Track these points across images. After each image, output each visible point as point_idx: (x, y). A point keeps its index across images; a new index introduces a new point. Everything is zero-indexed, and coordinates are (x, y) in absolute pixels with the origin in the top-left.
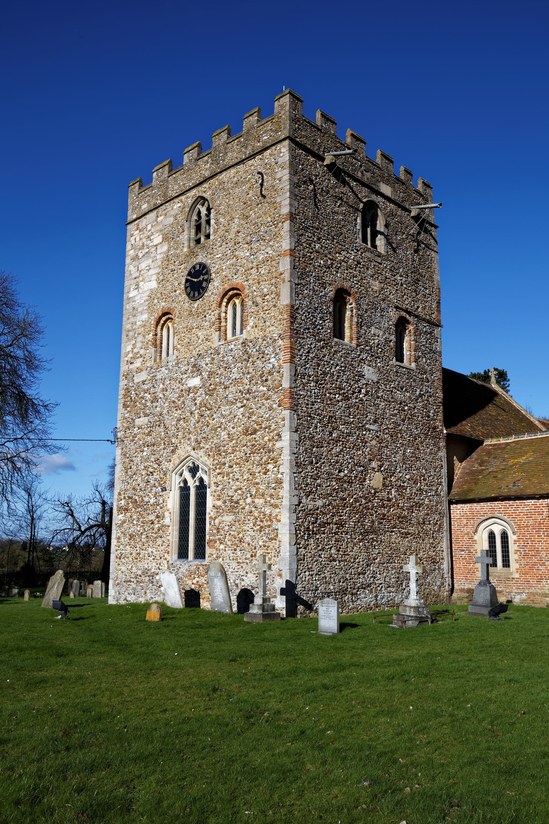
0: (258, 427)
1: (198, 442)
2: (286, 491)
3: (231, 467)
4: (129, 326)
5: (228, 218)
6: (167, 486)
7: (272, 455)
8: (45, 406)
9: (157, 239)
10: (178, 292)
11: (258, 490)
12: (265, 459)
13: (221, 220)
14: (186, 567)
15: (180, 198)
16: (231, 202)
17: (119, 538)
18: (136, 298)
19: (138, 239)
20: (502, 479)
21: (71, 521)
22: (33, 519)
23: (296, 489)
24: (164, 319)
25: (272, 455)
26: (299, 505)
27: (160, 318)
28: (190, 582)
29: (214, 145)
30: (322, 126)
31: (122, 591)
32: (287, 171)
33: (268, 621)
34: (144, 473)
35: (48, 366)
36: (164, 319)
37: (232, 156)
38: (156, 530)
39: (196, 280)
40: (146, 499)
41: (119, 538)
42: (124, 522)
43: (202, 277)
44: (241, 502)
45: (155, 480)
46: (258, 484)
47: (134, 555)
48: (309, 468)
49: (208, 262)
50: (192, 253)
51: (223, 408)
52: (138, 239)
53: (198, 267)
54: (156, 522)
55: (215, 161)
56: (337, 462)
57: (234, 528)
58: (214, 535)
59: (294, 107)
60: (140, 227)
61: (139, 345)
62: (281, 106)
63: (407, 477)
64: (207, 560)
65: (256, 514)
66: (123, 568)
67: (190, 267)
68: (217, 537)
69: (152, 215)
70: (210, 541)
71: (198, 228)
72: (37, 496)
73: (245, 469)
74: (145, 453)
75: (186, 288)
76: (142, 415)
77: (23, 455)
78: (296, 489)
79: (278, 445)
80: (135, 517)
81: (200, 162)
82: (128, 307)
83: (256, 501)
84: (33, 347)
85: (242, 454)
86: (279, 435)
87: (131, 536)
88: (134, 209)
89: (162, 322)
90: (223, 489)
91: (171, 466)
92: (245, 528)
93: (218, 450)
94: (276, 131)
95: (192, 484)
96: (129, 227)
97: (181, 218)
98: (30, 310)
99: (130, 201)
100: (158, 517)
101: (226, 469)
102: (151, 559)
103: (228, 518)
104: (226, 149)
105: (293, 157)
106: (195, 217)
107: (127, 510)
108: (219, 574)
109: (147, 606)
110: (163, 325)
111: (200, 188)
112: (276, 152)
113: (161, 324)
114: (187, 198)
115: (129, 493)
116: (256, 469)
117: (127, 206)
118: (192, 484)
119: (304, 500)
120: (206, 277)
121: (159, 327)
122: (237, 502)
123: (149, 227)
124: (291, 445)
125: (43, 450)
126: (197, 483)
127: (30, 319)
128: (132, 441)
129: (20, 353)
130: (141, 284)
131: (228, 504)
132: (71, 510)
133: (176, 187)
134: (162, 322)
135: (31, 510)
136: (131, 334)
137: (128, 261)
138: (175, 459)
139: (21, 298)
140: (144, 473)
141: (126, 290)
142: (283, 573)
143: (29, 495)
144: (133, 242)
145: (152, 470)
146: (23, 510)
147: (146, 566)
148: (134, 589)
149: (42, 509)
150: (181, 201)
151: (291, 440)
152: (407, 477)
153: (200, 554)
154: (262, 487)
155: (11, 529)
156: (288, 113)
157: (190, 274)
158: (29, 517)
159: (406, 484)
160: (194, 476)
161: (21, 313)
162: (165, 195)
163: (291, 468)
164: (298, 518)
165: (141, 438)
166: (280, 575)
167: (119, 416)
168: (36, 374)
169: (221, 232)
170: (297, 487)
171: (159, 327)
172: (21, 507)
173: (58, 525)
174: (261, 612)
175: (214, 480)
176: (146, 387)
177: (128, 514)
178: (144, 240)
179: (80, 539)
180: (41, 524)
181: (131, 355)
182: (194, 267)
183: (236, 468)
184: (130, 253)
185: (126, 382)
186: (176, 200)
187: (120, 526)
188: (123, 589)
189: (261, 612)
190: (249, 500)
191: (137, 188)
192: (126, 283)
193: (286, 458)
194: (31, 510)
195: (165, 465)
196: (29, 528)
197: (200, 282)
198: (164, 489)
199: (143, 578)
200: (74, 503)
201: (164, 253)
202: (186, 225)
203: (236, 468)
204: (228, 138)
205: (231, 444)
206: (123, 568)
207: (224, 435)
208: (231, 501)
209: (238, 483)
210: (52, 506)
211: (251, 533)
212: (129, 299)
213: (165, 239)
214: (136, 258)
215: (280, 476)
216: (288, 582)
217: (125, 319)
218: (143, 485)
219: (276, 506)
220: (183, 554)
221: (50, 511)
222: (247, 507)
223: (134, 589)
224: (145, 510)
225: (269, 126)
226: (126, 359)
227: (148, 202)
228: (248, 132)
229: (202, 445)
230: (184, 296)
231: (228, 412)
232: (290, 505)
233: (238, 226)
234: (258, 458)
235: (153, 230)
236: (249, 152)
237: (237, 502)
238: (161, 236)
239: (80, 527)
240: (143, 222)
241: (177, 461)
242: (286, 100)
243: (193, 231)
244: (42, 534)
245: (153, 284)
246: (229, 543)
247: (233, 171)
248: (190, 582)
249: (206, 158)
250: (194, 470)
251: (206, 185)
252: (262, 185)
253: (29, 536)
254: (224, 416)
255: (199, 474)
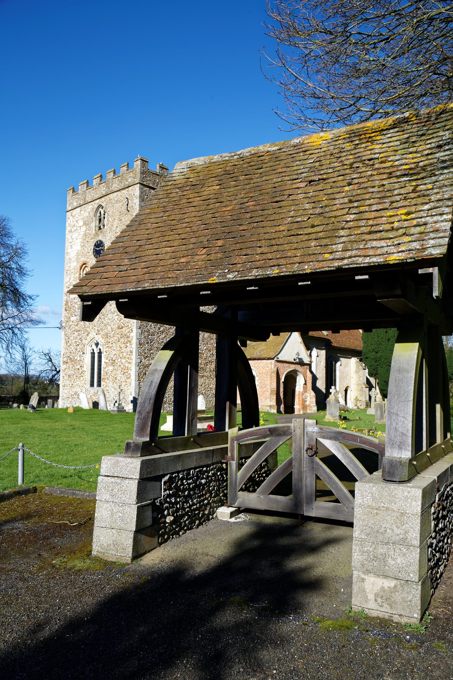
0: (123, 326)
1: (98, 331)
2: (134, 357)
3: (112, 344)
4: (67, 268)
5: (113, 219)
6: (85, 352)
7: (129, 339)
8: (30, 298)
9: (81, 223)
10: (90, 253)
11: (123, 355)
12: (126, 341)
13: (110, 219)
14: (93, 391)
15: (92, 203)
16: (114, 211)
17: (63, 377)
18: (71, 253)
19: (72, 221)
20: (256, 349)
21: (51, 365)
22: (26, 364)
23: (139, 355)
24: (84, 266)
25: (129, 339)
26: (141, 362)
27: (82, 266)
28: (94, 398)
29: (107, 178)
30: (160, 172)
31: (65, 403)
32: (138, 200)
33: (120, 413)
34: (75, 344)
35: (31, 274)
36: (84, 266)
37: (116, 185)
38: (80, 373)
39: (98, 249)
40: (76, 358)
41: (63, 377)
42: (66, 369)
43: (101, 248)
44: (116, 361)
45: (80, 348)
46: (123, 352)
47: (70, 385)
48: (147, 345)
49: (103, 240)
50: (97, 234)
51: (109, 315)
52: (72, 221)
53: (99, 243)
54: (80, 369)
55: (108, 187)
56: (162, 342)
57: (113, 373)
58: (105, 376)
59: (143, 166)
60: (73, 215)
61: (72, 279)
62: (137, 165)
63: (205, 348)
64: (102, 387)
65: (122, 367)
66: (66, 391)
67: (95, 241)
68: (106, 377)
69: (78, 209)
70: (103, 379)
71: (100, 220)
72: (28, 349)
73: (118, 345)
74: (75, 335)
75: (94, 252)
76: (73, 315)
77: (18, 326)
78: (139, 355)
79: (132, 335)
80: (70, 366)
81: (101, 186)
82: (67, 257)
83: (122, 360)
84: (22, 262)
85: (117, 338)
86: (132, 330)
87: (69, 376)
88: (70, 204)
89: (83, 268)
90: (109, 354)
91: (86, 342)
92: (118, 373)
93: (107, 336)
94: (134, 178)
95: (96, 351)
96: (68, 213)
97: (92, 214)
98: (19, 241)
99: (68, 199)
100: (81, 367)
101: (110, 345)
102: (78, 387)
103: (111, 368)
104: (112, 181)
105: (141, 192)
106: (98, 215)
107: (67, 363)
108: (102, 393)
109: (67, 408)
110: (84, 269)
111: (101, 200)
112: (134, 189)
113: (82, 269)
114: (95, 204)
115: (68, 355)
116: (123, 346)
117: (67, 202)
118: (96, 351)
119: (143, 361)
120: (102, 248)
121: (82, 270)
122: (114, 361)
123: (77, 216)
124: (136, 335)
125: (30, 323)
126: (98, 351)
127: (19, 246)
128: (69, 328)
129: (14, 266)
130: (73, 246)
131: (111, 361)
132: (50, 358)
133: (90, 197)
134: (83, 268)
135: (25, 358)
136: (68, 272)
137: (67, 232)
138: (89, 339)
139: (14, 231)
140: (75, 344)
141: (66, 248)
142: (132, 393)
143: (23, 349)
144: (69, 222)
145: (78, 344)
146: (20, 359)
147: (76, 390)
148: (71, 401)
149: (32, 358)
150: (92, 205)
151: (137, 333)
152: (205, 348)
153: (99, 385)
154: (125, 354)
155: (13, 370)
156: (139, 170)
157: (95, 245)
158: (24, 363)
159: (203, 352)
160: (97, 347)
161: (13, 242)
162: (85, 200)
163: (137, 345)
164: (140, 369)
165: (74, 327)
166: (131, 394)
167: (63, 315)
168: (24, 278)
169: (109, 226)
170: (140, 354)
171: (82, 270)
172: (18, 356)
173: (42, 367)
174: (117, 409)
175: (105, 350)
176: (75, 301)
177: (68, 365)
178: (75, 222)
179: (56, 376)
180: (31, 367)
181: (68, 283)
182: (97, 242)
183: (114, 344)
184: (68, 228)
185: (66, 297)
186: (90, 204)
187: (64, 371)
188: (66, 402)
189: (117, 409)
190: (119, 360)
191: (71, 192)
192: (66, 244)
193: (134, 341)
194: (25, 358)
195: (84, 341)
196: (24, 369)
197: (100, 250)
198: (84, 353)
199: (74, 396)
200: (52, 354)
201: (84, 231)
202: (94, 218)
203: (114, 344)
204: (114, 175)
205: (112, 333)
206: (66, 391)
207: (109, 328)
208: (112, 360)
209: (115, 352)
210: (39, 356)
211: (120, 375)
212: (67, 253)
213: (85, 224)
214: (70, 231)
215: (132, 349)
216: (134, 397)
217: (66, 264)
218: (74, 351)
219: (130, 363)
220: (92, 385)
221: (37, 358)
222: (118, 363)
223: (71, 401)
224: (75, 363)
225: (131, 174)
226: (66, 285)
227: (77, 201)
228: (122, 175)
229: (100, 332)
230: (93, 256)
231: (111, 318)
232: (136, 363)
233: (117, 224)
234: (123, 340)
235: (79, 218)
236: (122, 186)
237: (114, 361)
238: (82, 222)
239: (56, 369)
240: (75, 212)
241: (89, 340)
242: (139, 162)
243: (98, 222)
244: (31, 373)
245: (79, 248)
246: (111, 380)
247: (115, 194)
248: (94, 398)
249: (103, 184)
250: (97, 344)
251: (103, 199)
252: (127, 205)
253: (24, 374)
254: (109, 319)
255: (99, 347)
